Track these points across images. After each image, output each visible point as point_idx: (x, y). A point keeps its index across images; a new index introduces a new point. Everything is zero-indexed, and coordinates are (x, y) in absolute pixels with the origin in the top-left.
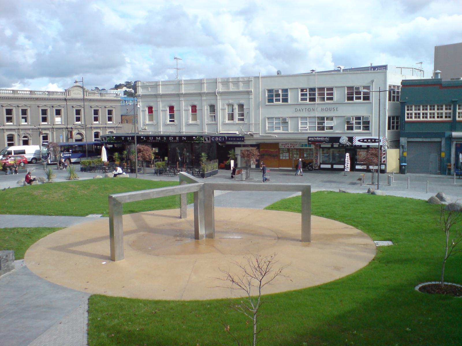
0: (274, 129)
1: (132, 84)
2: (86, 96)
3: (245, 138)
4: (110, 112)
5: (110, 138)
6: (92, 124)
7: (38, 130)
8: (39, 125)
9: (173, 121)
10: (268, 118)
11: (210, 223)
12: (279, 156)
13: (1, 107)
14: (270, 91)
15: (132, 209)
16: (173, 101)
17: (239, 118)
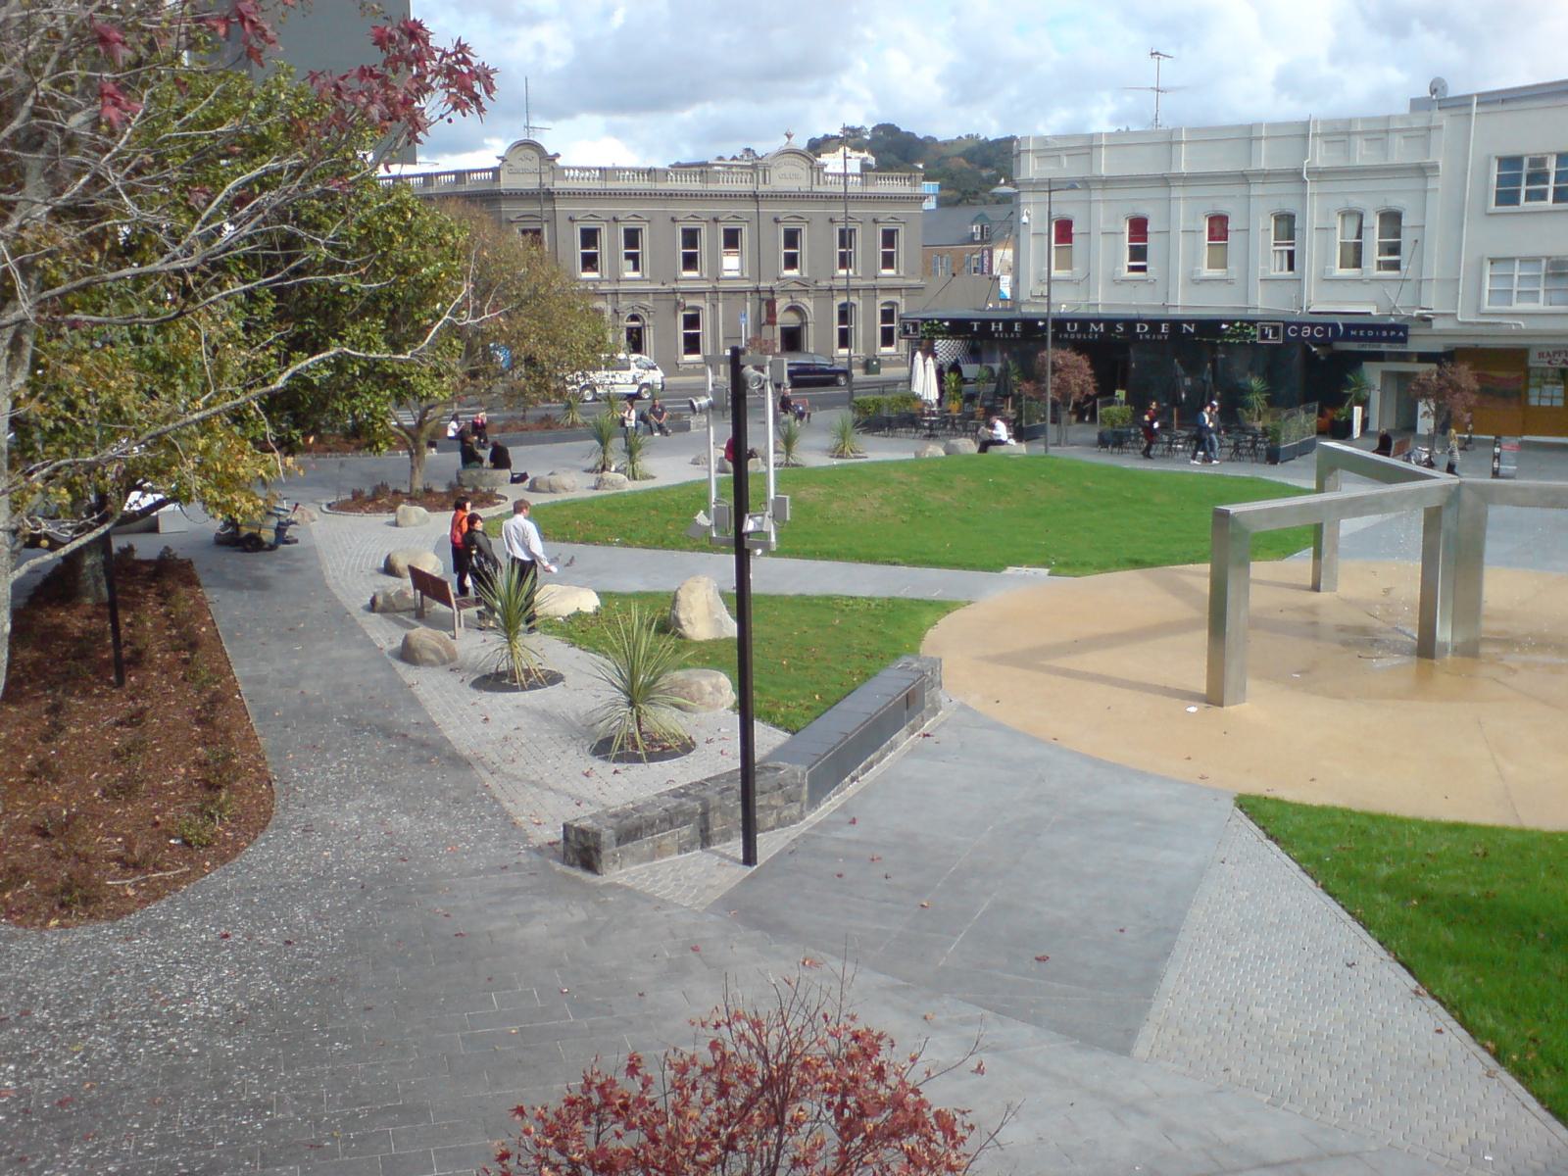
0: (1514, 300)
1: (868, 137)
2: (819, 183)
3: (1411, 331)
4: (889, 238)
5: (933, 324)
6: (676, 280)
7: (672, 296)
8: (676, 280)
9: (1143, 269)
10: (1493, 261)
11: (1469, 608)
12: (1527, 397)
13: (569, 223)
14: (1510, 163)
15: (1137, 557)
16: (1225, 197)
17: (1382, 258)
